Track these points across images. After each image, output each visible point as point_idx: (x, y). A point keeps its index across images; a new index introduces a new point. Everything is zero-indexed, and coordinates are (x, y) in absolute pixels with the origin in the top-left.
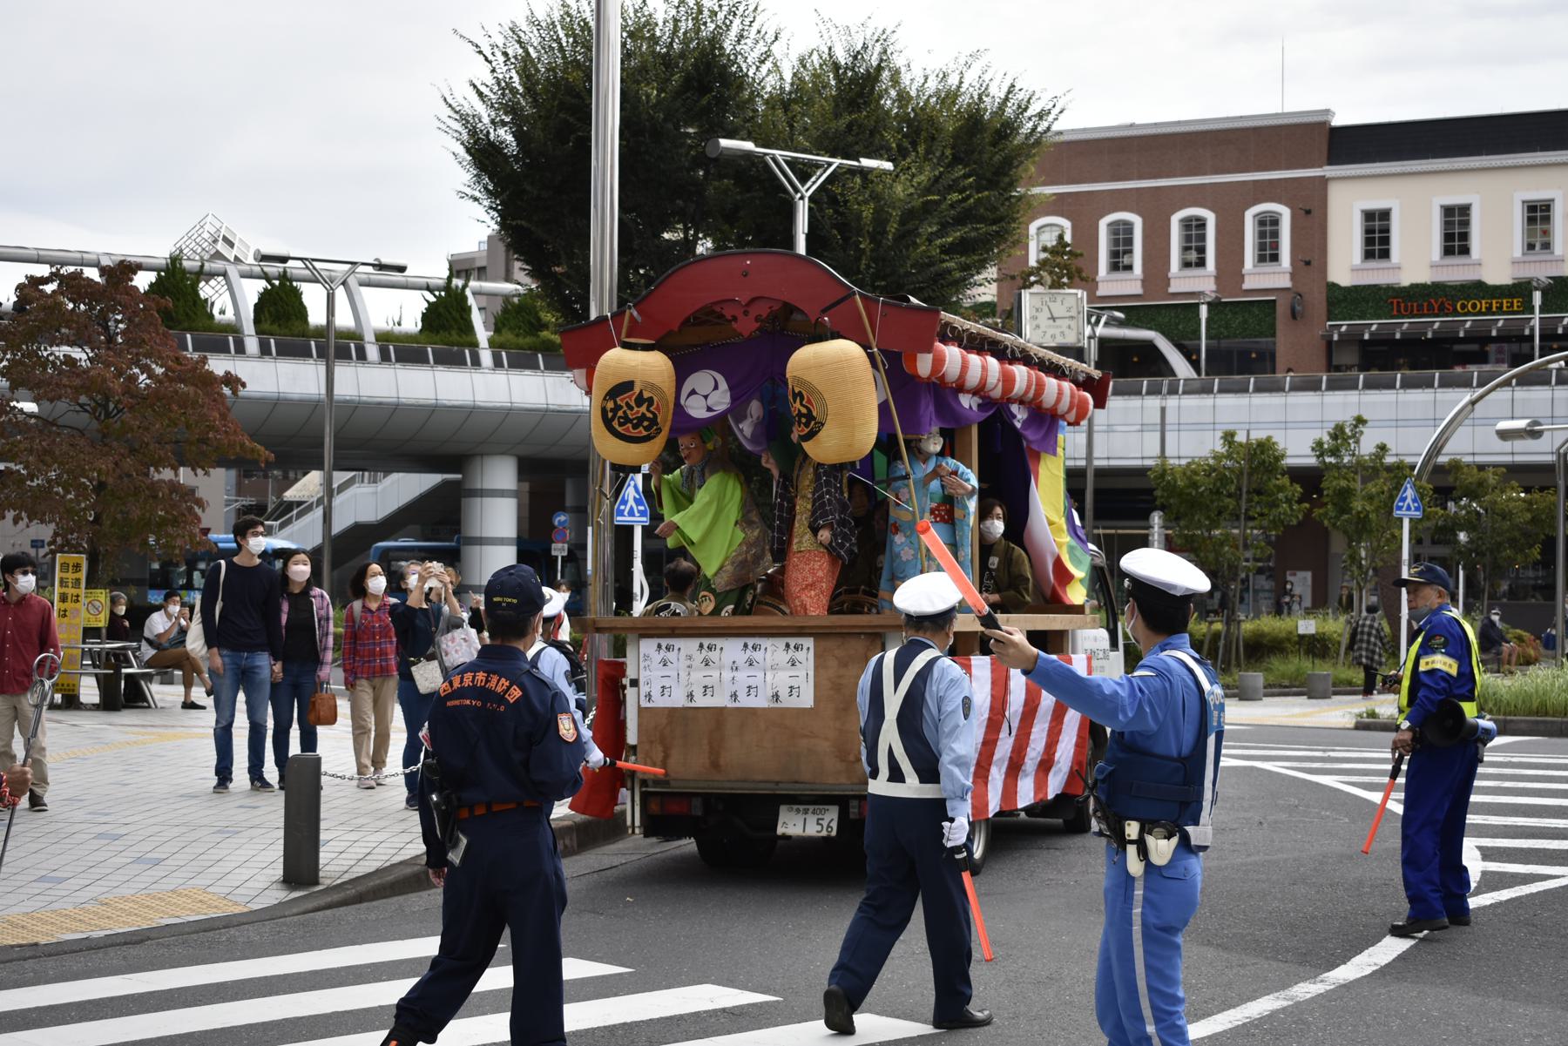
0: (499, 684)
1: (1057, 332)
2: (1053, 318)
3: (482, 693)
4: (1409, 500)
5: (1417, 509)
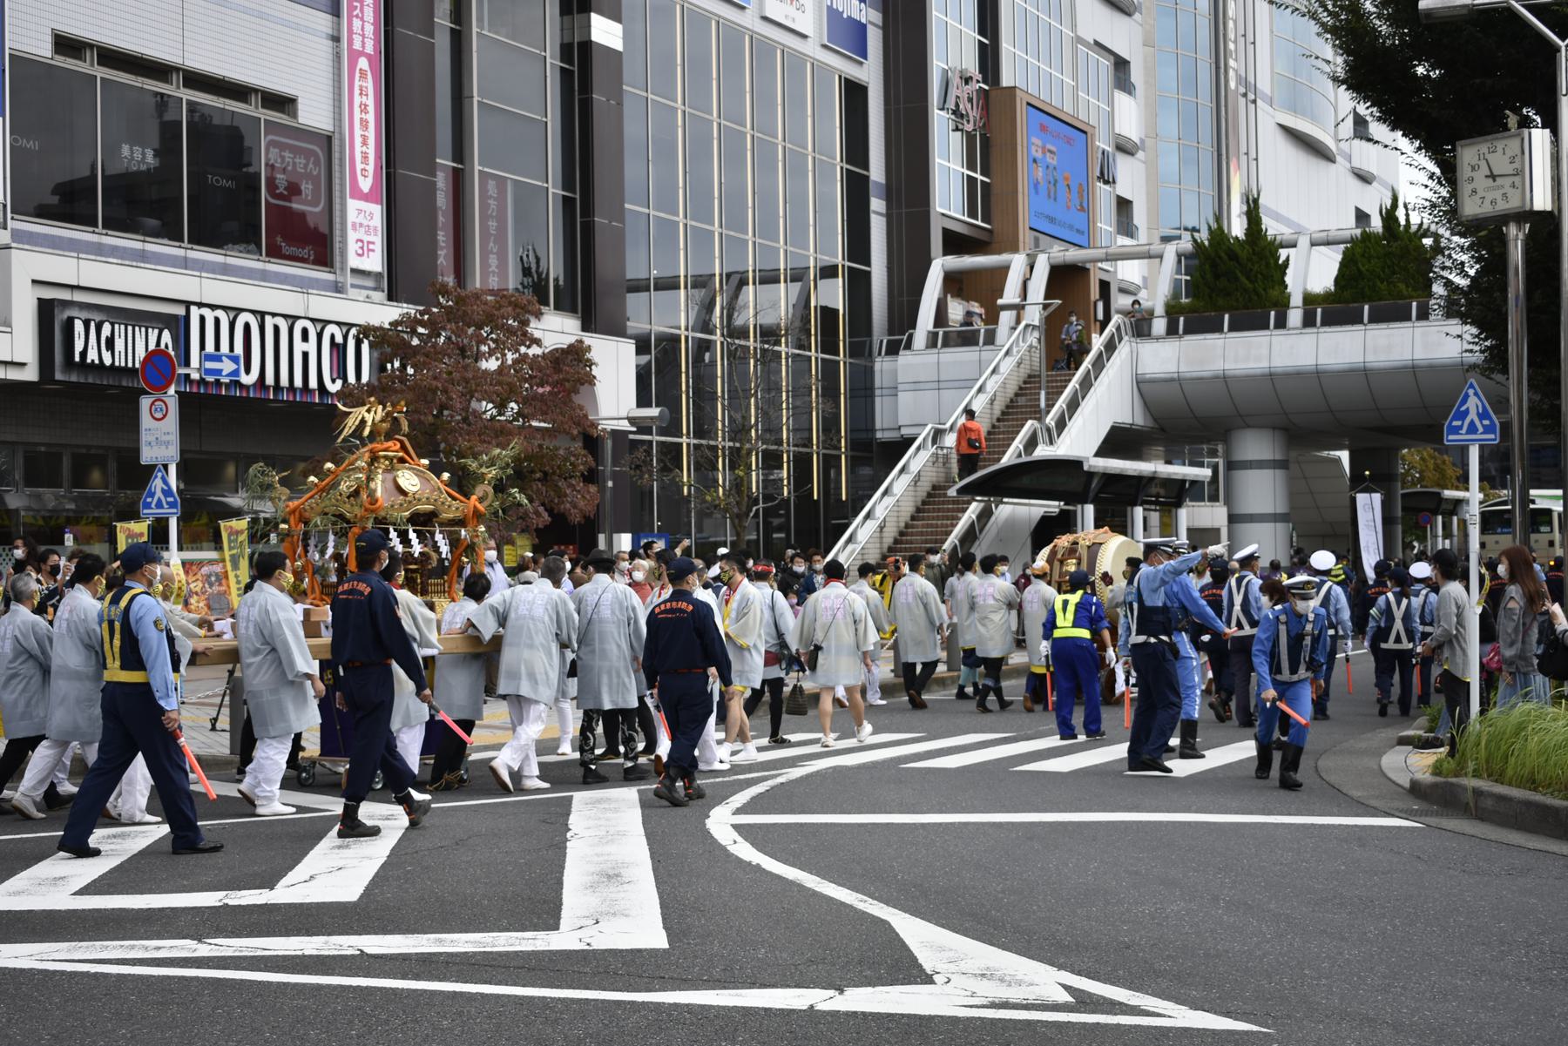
0: (683, 605)
1: (1498, 195)
2: (1493, 177)
3: (672, 611)
4: (1473, 416)
5: (1487, 430)
